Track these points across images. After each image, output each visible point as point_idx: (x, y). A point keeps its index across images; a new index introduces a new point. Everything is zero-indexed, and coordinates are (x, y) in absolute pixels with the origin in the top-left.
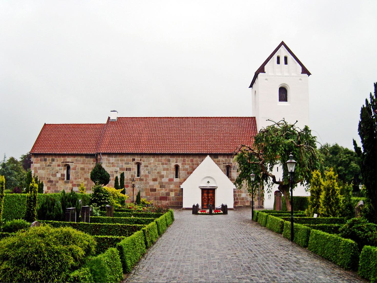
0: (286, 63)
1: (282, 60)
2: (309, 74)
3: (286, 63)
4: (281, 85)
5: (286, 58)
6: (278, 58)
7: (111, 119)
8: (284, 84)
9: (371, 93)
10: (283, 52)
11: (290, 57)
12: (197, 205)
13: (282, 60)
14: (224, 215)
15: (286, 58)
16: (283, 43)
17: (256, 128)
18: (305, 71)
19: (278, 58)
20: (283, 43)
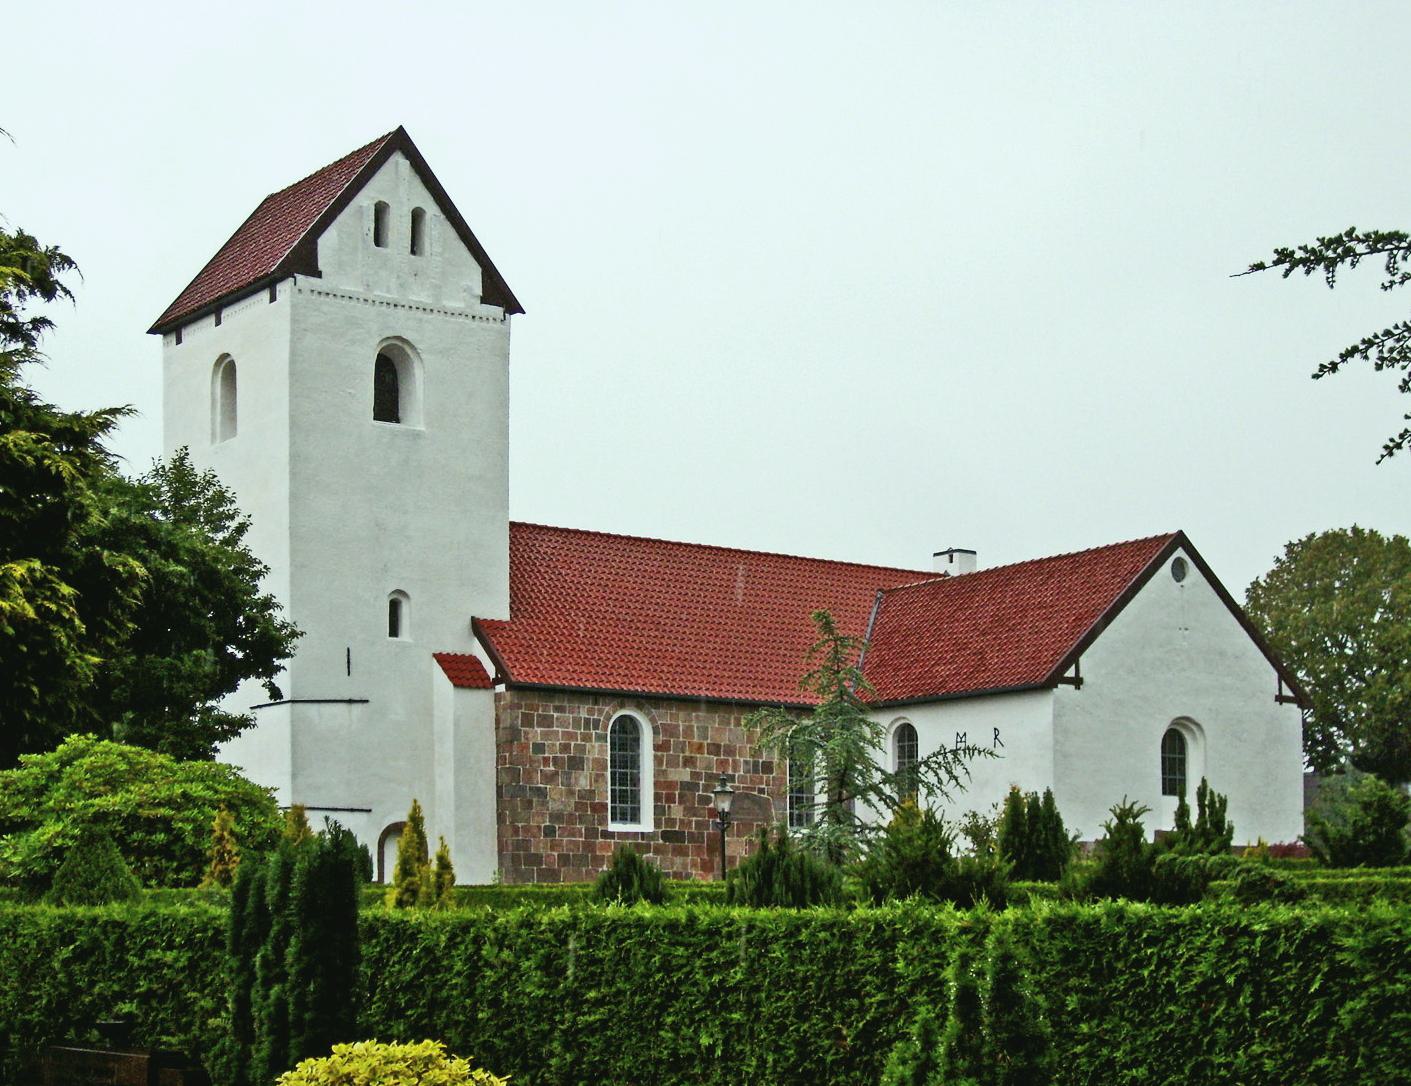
0: (415, 247)
1: (399, 227)
2: (512, 306)
3: (415, 247)
4: (384, 344)
5: (417, 216)
6: (381, 210)
7: (245, 541)
8: (399, 338)
9: (367, 701)
10: (394, 183)
11: (435, 223)
12: (240, 734)
13: (399, 227)
14: (470, 626)
15: (417, 216)
16: (399, 142)
17: (1057, 716)
18: (497, 293)
19: (381, 210)
20: (399, 142)
